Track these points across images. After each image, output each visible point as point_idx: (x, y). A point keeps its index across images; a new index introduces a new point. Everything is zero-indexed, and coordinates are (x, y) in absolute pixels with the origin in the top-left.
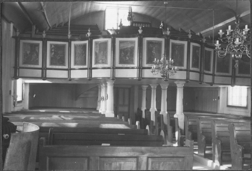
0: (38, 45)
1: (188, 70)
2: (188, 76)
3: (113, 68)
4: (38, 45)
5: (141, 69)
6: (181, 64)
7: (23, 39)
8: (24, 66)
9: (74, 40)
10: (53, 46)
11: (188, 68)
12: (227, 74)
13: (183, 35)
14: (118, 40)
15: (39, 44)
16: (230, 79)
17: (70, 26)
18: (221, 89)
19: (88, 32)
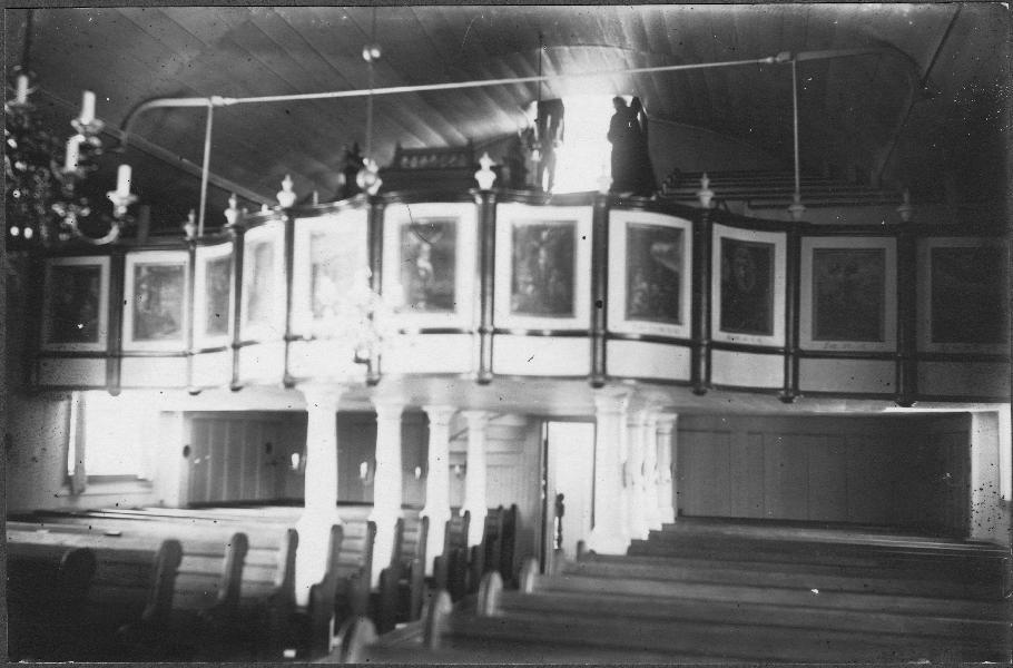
0: (96, 271)
1: (600, 335)
2: (599, 358)
3: (482, 331)
4: (96, 271)
5: (487, 338)
6: (565, 307)
7: (815, 235)
8: (53, 347)
9: (137, 248)
10: (144, 272)
11: (600, 324)
12: (871, 346)
13: (727, 190)
14: (619, 221)
15: (773, 245)
16: (888, 368)
17: (801, 185)
18: (976, 425)
19: (187, 220)
